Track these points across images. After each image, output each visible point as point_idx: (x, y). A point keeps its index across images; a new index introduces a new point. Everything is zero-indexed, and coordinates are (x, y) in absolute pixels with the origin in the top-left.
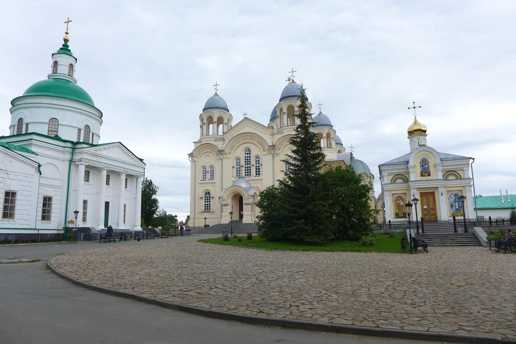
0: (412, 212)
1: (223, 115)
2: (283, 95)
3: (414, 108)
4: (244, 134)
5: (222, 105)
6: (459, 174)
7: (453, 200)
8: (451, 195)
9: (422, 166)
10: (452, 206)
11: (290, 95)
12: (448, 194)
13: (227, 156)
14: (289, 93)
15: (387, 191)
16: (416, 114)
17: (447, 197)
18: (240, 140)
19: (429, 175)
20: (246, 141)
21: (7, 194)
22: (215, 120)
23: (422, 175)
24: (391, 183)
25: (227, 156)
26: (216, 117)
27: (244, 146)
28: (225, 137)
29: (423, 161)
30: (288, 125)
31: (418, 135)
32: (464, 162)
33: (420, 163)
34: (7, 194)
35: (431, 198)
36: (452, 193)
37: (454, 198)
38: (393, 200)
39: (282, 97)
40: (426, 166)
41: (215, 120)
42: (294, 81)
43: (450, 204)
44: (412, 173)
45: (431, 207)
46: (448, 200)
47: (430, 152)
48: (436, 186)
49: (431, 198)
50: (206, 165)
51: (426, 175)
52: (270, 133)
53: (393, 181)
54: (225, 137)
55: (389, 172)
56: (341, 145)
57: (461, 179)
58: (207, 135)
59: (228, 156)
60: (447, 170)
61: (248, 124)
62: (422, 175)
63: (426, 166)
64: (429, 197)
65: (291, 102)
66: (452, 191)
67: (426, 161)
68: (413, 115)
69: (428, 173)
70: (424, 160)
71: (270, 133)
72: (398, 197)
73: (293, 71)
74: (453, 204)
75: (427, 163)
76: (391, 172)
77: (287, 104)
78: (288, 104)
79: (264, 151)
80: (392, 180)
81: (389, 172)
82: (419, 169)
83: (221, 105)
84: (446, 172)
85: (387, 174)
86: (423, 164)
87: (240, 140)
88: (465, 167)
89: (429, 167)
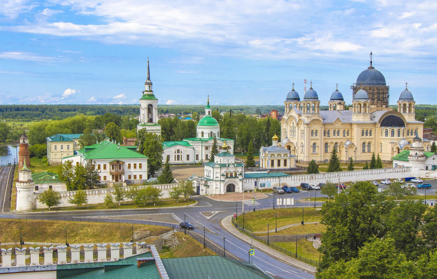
21: (187, 155)
34: (187, 155)
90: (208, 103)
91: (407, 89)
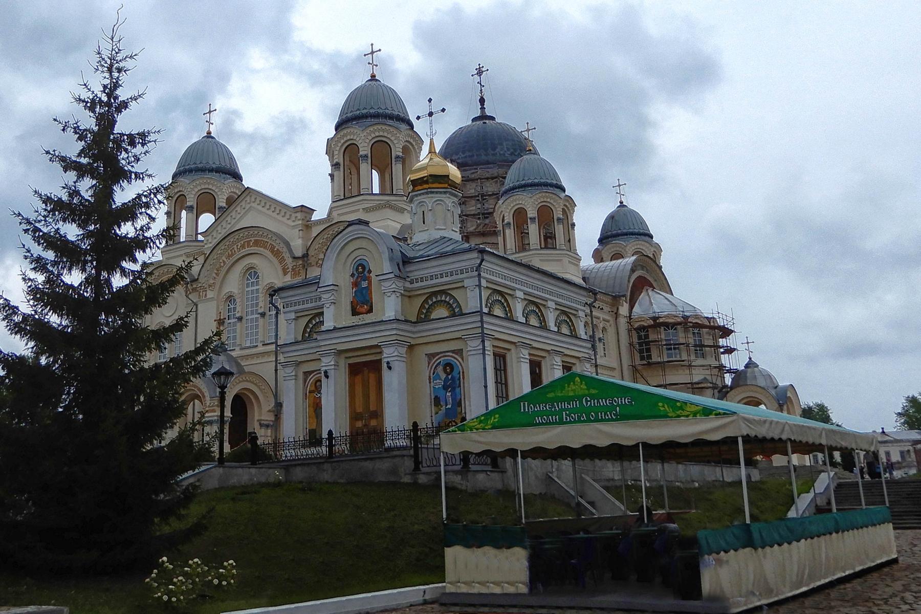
0: (682, 437)
1: (210, 187)
2: (347, 113)
3: (431, 114)
4: (236, 233)
5: (226, 164)
6: (454, 297)
7: (439, 383)
8: (435, 368)
9: (356, 284)
10: (437, 401)
11: (380, 111)
12: (429, 363)
13: (206, 295)
14: (361, 107)
15: (286, 365)
16: (434, 133)
17: (428, 374)
18: (236, 250)
19: (370, 310)
20: (247, 249)
22: (191, 201)
23: (355, 313)
24: (304, 340)
25: (206, 295)
26: (193, 196)
27: (245, 265)
28: (206, 244)
29: (357, 269)
30: (344, 196)
31: (423, 194)
32: (464, 264)
33: (353, 275)
35: (372, 377)
36: (439, 361)
37: (443, 376)
38: (306, 390)
39: (344, 117)
40: (364, 284)
41: (191, 201)
42: (212, 135)
43: (433, 397)
44: (328, 306)
45: (372, 408)
46: (430, 383)
47: (359, 238)
48: (374, 342)
49: (372, 377)
50: (166, 322)
51: (364, 310)
52: (300, 222)
53: (307, 335)
54: (206, 244)
55: (297, 308)
56: (647, 238)
57: (462, 314)
58: (345, 198)
59: (210, 294)
60: (426, 291)
61: (253, 205)
62: (355, 313)
63: (364, 284)
64: (369, 377)
65: (383, 131)
66: (438, 354)
67: (364, 268)
68: (427, 135)
69: (369, 304)
70: (359, 265)
71: (300, 222)
72: (316, 383)
73: (374, 50)
74: (441, 394)
75: (367, 275)
76: (301, 307)
77: (373, 135)
78: (377, 134)
79: (285, 273)
80: (305, 331)
81: (297, 308)
82: (347, 296)
83: (211, 163)
84: (311, 316)
85: (293, 316)
86: (357, 278)
87: (236, 250)
88: (468, 278)
89: (370, 284)
90: (482, 101)
91: (483, 117)
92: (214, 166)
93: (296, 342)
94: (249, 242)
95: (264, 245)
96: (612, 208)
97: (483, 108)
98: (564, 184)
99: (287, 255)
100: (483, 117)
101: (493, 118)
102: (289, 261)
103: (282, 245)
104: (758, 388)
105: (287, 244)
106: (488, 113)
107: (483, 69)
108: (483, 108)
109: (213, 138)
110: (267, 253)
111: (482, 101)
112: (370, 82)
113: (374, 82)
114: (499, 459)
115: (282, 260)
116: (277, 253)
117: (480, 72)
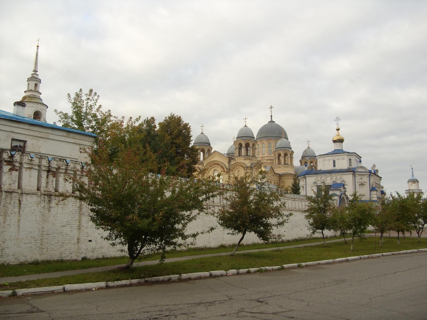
61: (217, 155)
90: (271, 116)
91: (272, 122)
92: (205, 142)
93: (245, 156)
94: (215, 164)
95: (219, 165)
96: (306, 148)
97: (271, 119)
98: (292, 147)
99: (225, 168)
100: (272, 122)
101: (274, 122)
102: (225, 169)
103: (224, 166)
104: (423, 253)
105: (225, 165)
106: (273, 120)
107: (272, 107)
108: (271, 119)
109: (203, 134)
110: (220, 167)
111: (271, 116)
112: (245, 127)
113: (246, 127)
114: (326, 185)
115: (223, 169)
116: (222, 167)
117: (271, 108)
